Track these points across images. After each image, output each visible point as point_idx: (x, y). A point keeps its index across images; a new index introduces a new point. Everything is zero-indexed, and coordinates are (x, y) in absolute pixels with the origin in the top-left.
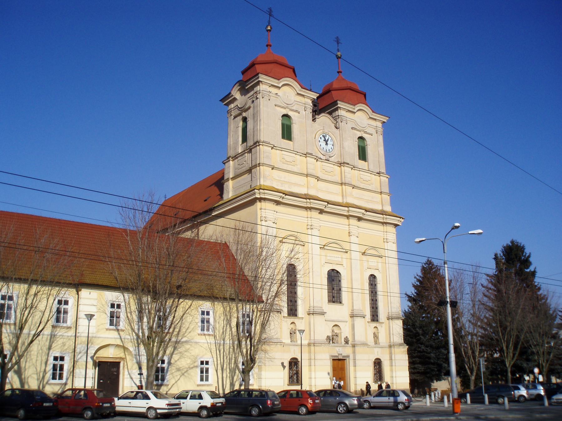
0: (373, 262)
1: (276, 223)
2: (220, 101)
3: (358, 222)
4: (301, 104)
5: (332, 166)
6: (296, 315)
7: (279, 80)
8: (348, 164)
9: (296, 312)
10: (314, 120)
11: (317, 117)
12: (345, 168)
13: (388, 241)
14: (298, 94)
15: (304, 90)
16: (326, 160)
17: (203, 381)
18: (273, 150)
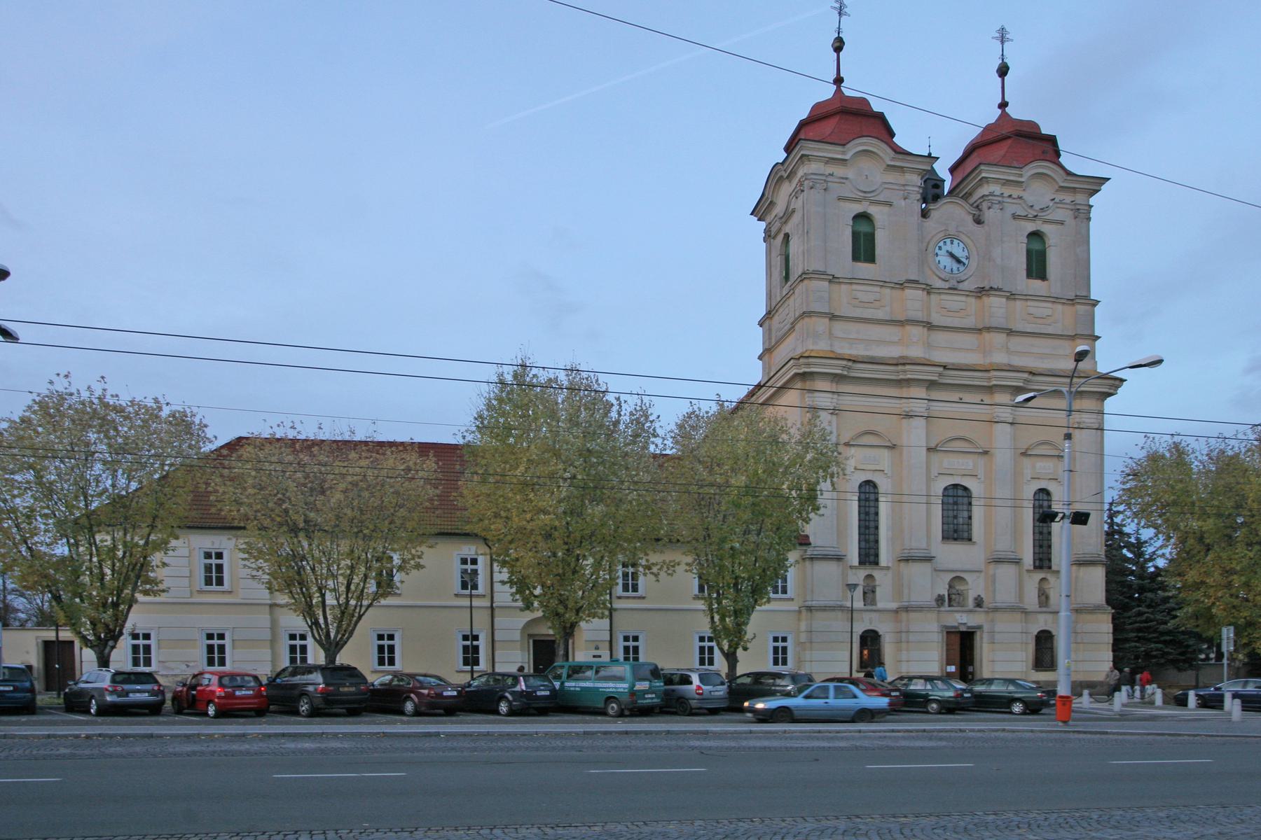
0: (1045, 466)
2: (752, 214)
3: (510, 356)
4: (897, 188)
5: (963, 298)
6: (877, 563)
7: (844, 145)
8: (998, 289)
10: (925, 214)
12: (992, 299)
16: (950, 289)
17: (778, 665)
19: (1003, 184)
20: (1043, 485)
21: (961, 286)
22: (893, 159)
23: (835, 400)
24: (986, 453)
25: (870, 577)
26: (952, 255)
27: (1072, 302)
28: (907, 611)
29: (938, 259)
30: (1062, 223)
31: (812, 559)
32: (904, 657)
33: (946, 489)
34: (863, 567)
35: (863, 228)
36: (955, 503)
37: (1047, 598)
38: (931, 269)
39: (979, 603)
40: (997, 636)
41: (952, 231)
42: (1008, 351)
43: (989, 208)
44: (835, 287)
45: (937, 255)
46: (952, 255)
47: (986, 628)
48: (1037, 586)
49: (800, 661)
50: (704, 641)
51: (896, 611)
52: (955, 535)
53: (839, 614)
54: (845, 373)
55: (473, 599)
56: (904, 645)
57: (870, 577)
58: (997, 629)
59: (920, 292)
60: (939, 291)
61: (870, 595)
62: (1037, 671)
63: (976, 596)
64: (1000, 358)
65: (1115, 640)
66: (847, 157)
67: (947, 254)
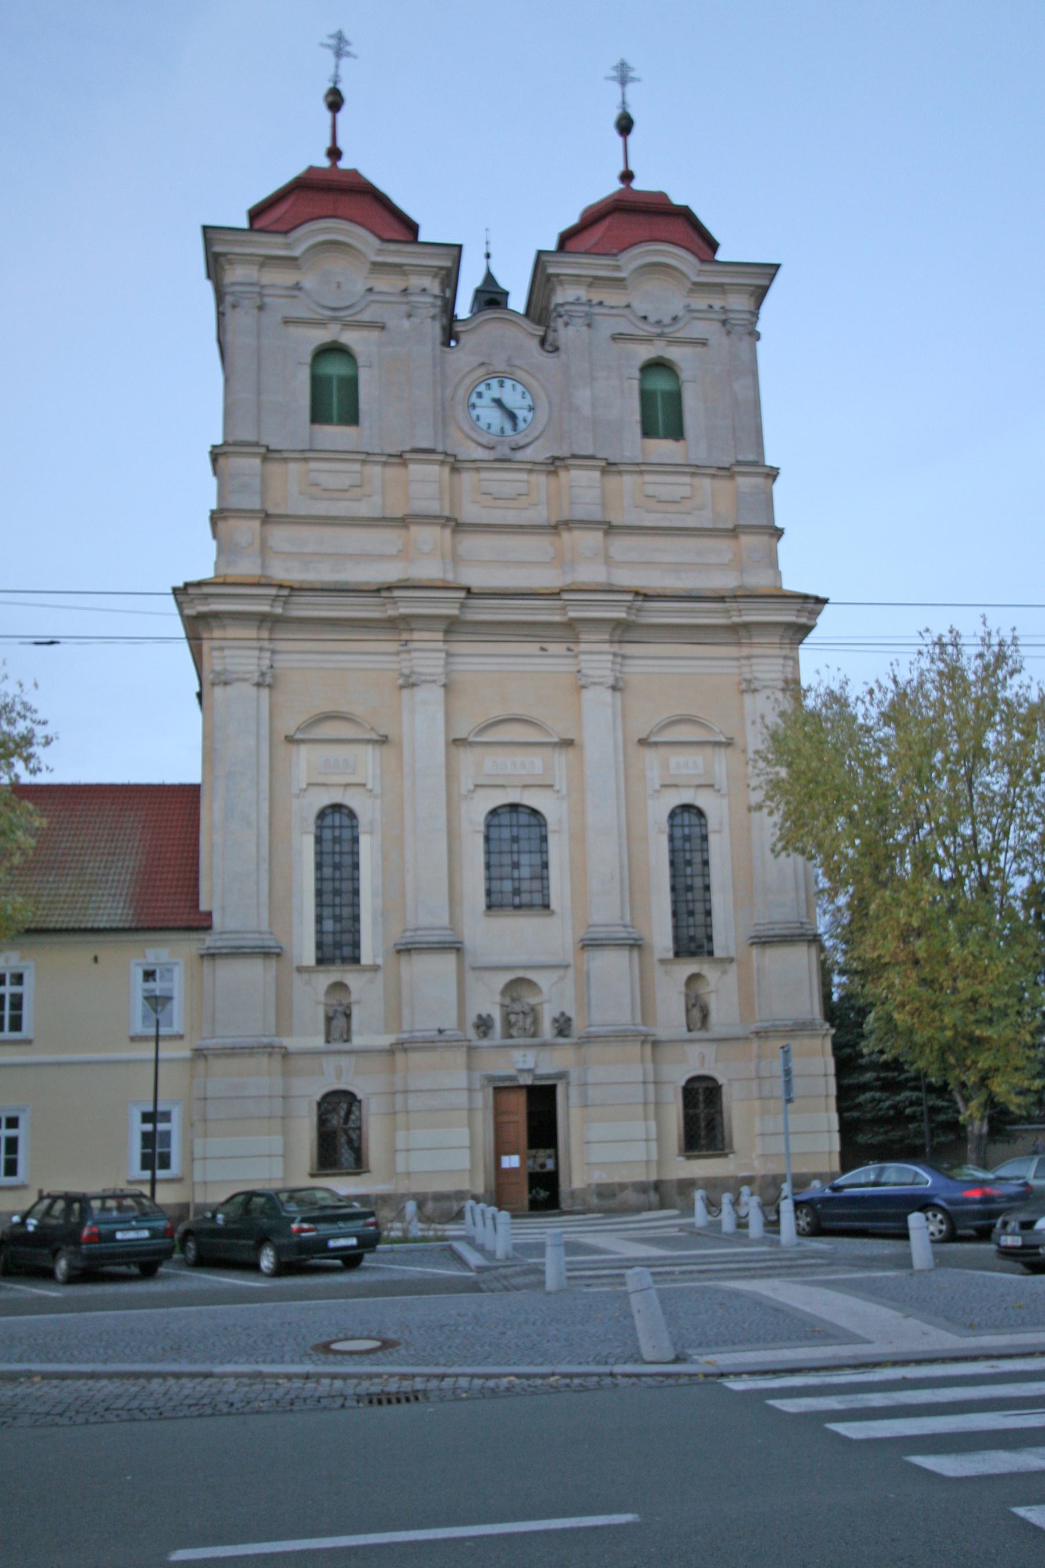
5: (524, 476)
6: (356, 960)
9: (356, 951)
12: (574, 473)
13: (756, 685)
15: (392, 247)
16: (497, 460)
19: (590, 285)
20: (686, 797)
21: (519, 455)
22: (380, 252)
23: (618, 667)
24: (567, 743)
25: (694, 979)
26: (498, 402)
27: (727, 472)
28: (405, 1050)
29: (475, 413)
30: (703, 343)
31: (213, 956)
33: (494, 812)
34: (322, 968)
35: (660, 383)
37: (705, 1016)
38: (462, 430)
39: (563, 1026)
40: (593, 1093)
41: (500, 365)
42: (608, 561)
43: (566, 324)
44: (613, 481)
45: (474, 406)
46: (498, 402)
47: (574, 1077)
48: (683, 989)
49: (190, 1159)
51: (391, 1051)
52: (517, 900)
53: (265, 1060)
54: (279, 610)
55: (161, 1044)
56: (401, 1118)
57: (340, 986)
58: (591, 1079)
59: (436, 468)
60: (477, 466)
61: (339, 1022)
62: (689, 1158)
63: (557, 1015)
64: (591, 573)
65: (840, 1088)
66: (297, 252)
67: (493, 404)
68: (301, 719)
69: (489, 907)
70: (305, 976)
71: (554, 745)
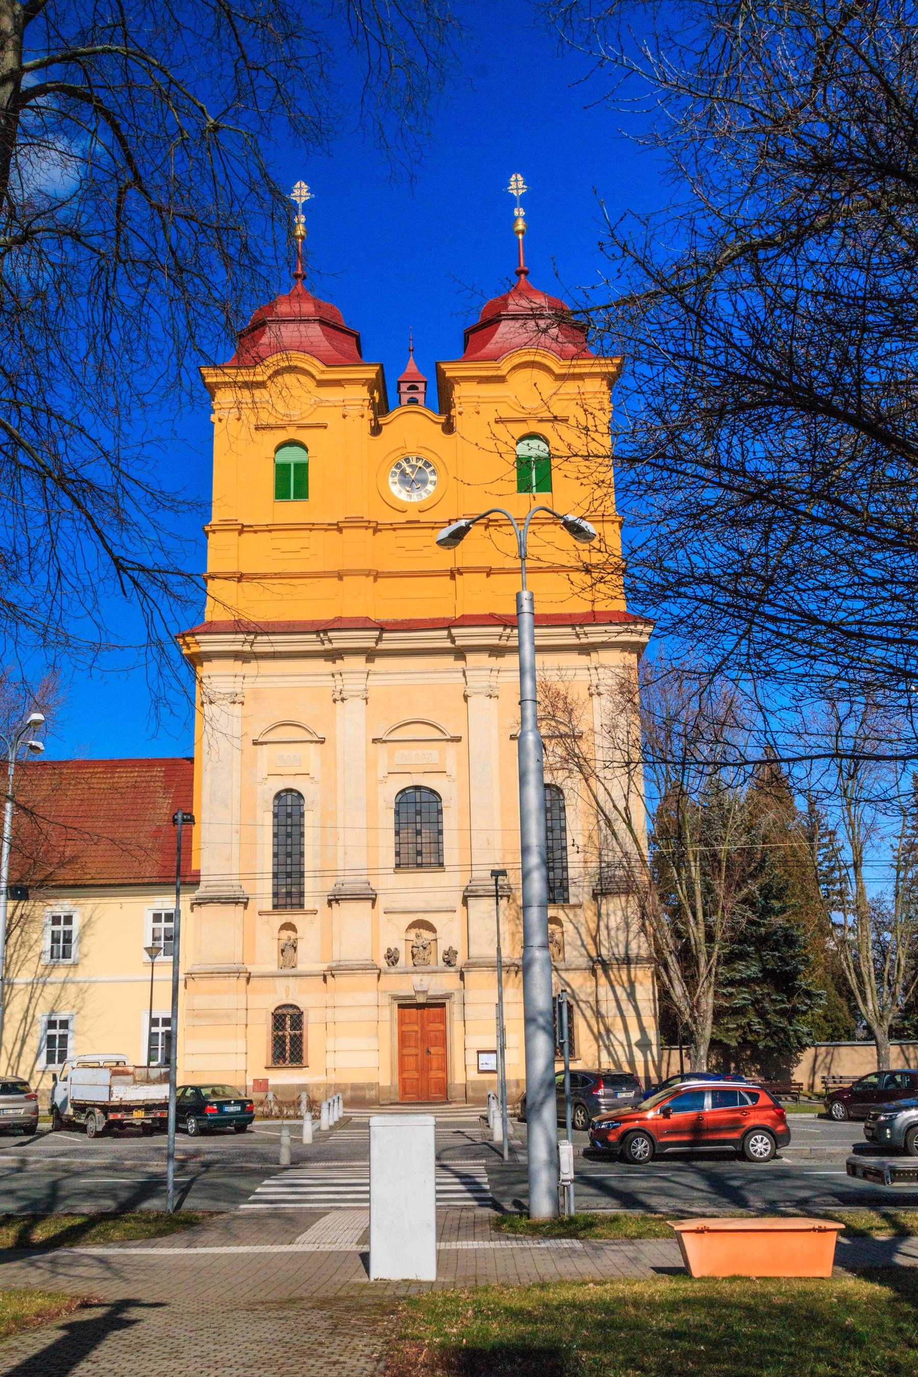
1: (242, 703)
6: (301, 906)
10: (376, 430)
11: (381, 421)
13: (344, 695)
14: (321, 383)
18: (244, 535)
24: (322, 741)
32: (330, 1048)
36: (418, 813)
50: (157, 1025)
53: (233, 981)
61: (289, 952)
68: (266, 725)
69: (398, 866)
70: (265, 917)
71: (448, 740)
